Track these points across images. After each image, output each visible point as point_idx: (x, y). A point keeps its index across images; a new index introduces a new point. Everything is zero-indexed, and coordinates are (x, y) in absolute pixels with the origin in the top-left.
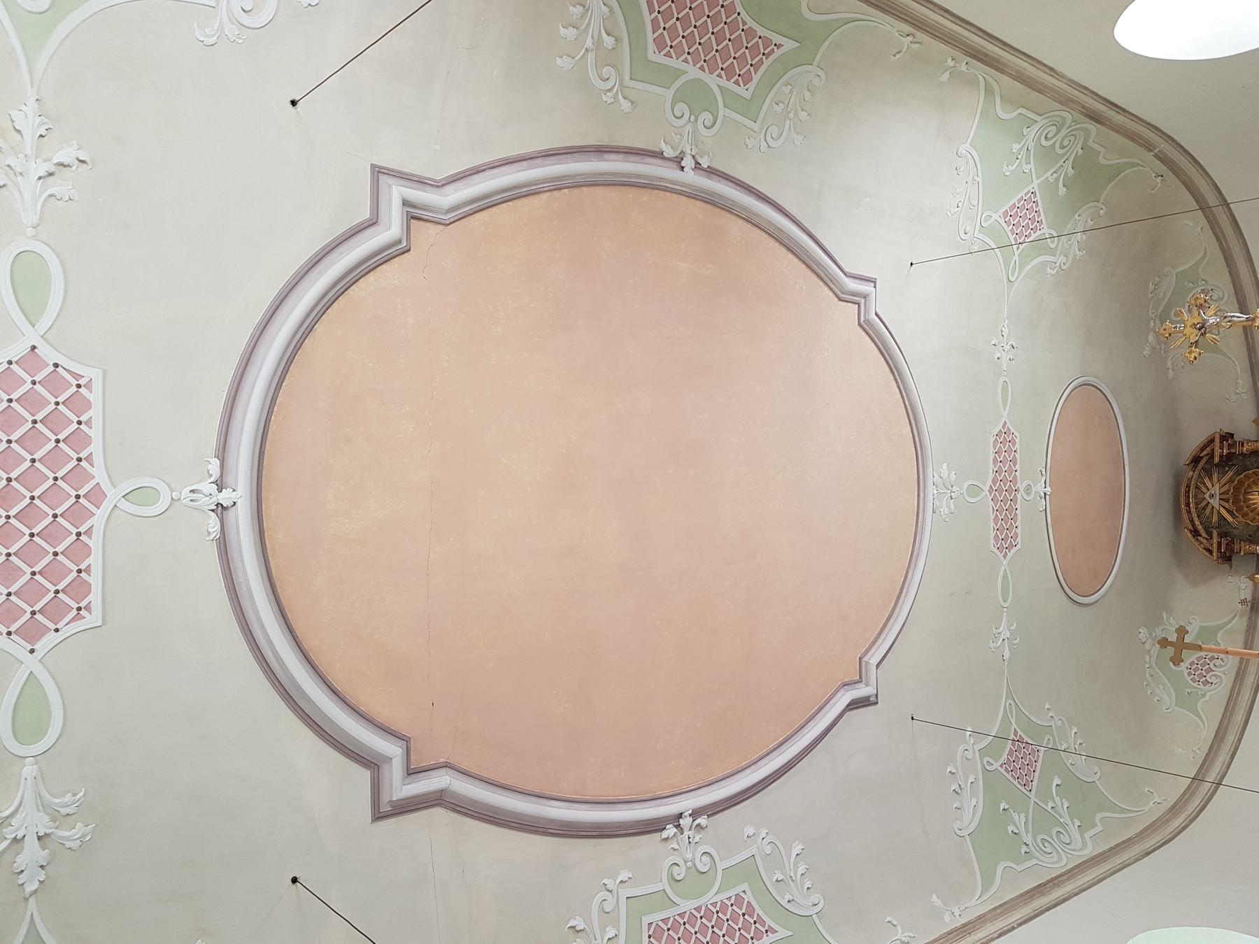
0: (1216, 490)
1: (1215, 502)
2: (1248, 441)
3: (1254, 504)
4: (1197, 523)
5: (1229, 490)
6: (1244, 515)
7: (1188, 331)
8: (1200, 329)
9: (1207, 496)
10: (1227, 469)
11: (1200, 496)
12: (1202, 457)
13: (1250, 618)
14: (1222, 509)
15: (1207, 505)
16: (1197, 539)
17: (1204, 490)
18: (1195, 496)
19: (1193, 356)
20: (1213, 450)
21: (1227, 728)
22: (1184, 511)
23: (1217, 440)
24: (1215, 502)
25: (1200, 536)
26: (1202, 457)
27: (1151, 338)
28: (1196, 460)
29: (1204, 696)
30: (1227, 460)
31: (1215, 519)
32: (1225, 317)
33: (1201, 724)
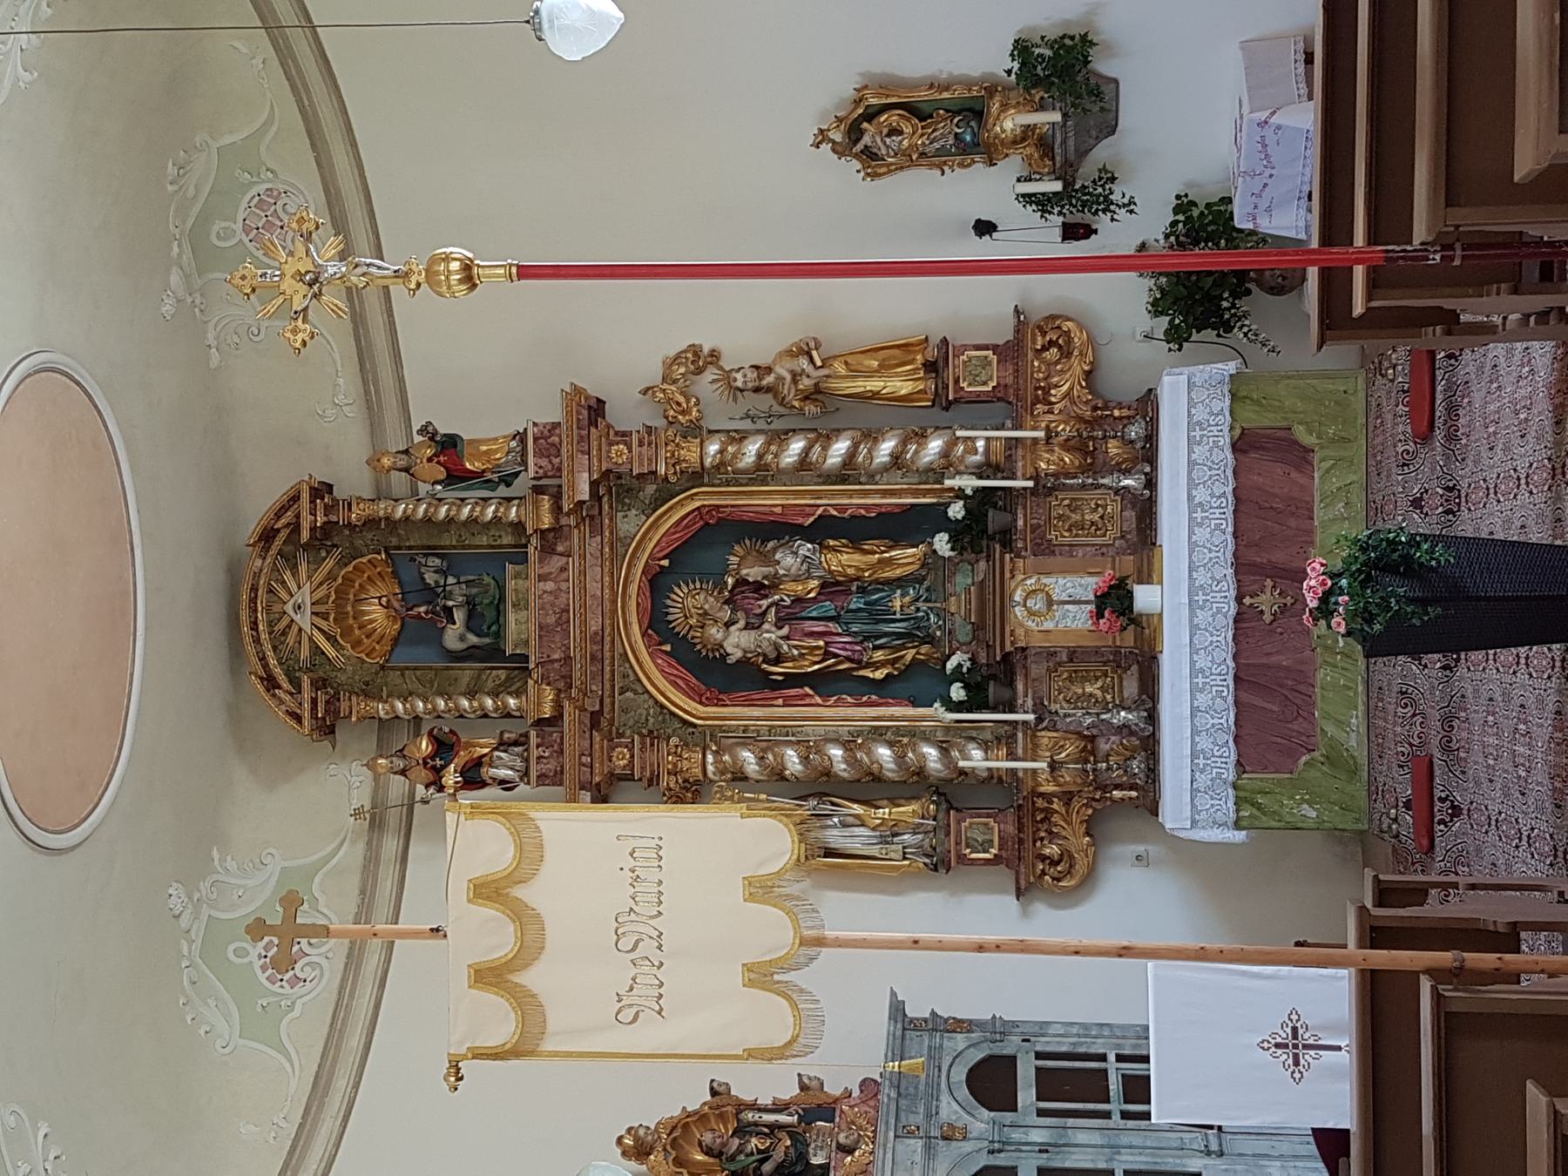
0: (305, 596)
1: (304, 620)
2: (360, 499)
3: (372, 621)
4: (272, 662)
5: (328, 596)
6: (357, 644)
7: (288, 285)
8: (310, 285)
9: (289, 608)
10: (324, 554)
11: (277, 608)
12: (278, 530)
13: (369, 843)
14: (316, 632)
15: (289, 626)
16: (274, 695)
17: (283, 595)
18: (268, 609)
19: (300, 337)
20: (298, 516)
21: (335, 1061)
22: (248, 640)
23: (305, 497)
24: (304, 620)
25: (279, 687)
26: (278, 530)
27: (175, 278)
28: (267, 536)
29: (291, 1007)
30: (324, 536)
31: (305, 652)
32: (356, 266)
33: (287, 1065)
